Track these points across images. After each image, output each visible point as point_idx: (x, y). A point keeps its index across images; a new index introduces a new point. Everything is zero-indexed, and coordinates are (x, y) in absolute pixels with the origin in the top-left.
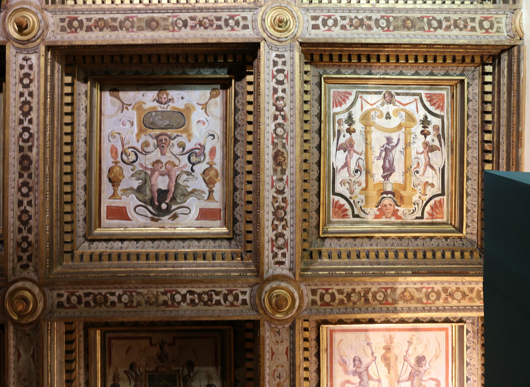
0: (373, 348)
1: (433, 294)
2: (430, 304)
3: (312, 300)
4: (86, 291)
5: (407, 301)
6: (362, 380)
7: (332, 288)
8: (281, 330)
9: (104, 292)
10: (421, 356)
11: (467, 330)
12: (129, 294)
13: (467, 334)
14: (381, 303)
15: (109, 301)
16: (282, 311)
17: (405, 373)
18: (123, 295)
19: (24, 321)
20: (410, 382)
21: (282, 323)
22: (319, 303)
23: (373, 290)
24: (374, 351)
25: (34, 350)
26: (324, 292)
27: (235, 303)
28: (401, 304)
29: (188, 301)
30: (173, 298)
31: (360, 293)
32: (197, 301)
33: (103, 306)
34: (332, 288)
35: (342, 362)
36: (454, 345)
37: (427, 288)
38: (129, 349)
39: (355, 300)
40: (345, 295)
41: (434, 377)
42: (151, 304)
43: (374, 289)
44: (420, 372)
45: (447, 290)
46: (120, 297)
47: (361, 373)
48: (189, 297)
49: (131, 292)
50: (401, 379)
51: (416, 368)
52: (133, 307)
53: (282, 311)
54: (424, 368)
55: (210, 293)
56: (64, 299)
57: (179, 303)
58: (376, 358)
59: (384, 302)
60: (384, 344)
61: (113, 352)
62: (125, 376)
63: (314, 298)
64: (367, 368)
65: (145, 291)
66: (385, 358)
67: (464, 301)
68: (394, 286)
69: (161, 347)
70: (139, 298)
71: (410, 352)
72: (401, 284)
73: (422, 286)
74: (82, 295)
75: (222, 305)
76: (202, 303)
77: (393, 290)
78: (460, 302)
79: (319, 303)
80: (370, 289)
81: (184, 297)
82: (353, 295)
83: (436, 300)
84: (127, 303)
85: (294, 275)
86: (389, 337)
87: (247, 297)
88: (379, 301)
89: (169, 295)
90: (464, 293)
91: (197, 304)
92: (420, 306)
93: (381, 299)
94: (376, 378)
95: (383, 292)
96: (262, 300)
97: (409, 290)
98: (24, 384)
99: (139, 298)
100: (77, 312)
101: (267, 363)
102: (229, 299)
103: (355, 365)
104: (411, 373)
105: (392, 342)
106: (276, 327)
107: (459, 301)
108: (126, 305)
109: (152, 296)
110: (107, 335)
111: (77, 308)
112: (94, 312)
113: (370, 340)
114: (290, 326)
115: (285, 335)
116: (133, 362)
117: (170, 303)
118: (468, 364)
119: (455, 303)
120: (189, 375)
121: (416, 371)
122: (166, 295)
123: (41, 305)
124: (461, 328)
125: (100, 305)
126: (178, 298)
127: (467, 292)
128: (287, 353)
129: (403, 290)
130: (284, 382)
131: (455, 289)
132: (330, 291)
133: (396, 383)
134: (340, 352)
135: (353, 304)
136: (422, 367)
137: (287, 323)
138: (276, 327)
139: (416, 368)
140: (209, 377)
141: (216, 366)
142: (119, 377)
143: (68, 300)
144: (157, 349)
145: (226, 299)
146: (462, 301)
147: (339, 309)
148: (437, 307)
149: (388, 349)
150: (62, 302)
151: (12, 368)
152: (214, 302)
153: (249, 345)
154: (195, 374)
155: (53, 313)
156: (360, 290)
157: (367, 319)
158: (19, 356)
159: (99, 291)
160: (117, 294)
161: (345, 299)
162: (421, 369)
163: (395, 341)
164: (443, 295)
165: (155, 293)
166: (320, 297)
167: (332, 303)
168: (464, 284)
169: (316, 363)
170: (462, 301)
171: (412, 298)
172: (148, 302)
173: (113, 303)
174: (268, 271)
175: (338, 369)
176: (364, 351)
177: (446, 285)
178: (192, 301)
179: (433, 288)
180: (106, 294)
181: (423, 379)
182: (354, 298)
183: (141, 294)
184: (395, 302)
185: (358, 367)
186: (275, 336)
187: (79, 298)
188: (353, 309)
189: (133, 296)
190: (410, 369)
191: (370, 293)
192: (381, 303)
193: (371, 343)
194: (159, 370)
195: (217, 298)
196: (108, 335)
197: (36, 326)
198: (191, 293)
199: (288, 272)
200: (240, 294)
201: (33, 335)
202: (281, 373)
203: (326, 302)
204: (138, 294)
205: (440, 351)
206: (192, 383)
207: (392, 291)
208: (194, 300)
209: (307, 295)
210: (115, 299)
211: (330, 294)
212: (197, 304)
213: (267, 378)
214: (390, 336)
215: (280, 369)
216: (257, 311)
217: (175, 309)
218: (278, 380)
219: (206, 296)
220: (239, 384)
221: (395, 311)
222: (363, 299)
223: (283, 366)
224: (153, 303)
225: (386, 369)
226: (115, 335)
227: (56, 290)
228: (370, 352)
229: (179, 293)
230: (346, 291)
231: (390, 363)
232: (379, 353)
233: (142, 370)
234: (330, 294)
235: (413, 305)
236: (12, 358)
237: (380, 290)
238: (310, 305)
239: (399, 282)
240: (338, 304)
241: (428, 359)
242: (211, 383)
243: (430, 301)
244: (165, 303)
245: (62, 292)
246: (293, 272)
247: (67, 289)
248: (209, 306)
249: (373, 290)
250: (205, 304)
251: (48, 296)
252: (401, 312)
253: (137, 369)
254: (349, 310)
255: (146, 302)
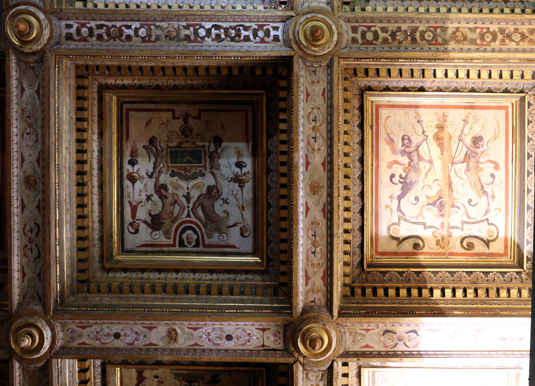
0: (424, 126)
1: (489, 34)
2: (485, 45)
3: (353, 38)
4: (99, 23)
5: (460, 41)
6: (411, 160)
7: (375, 26)
8: (317, 69)
9: (118, 24)
10: (478, 136)
11: (529, 102)
12: (147, 27)
13: (529, 107)
14: (429, 43)
15: (125, 35)
16: (318, 43)
17: (460, 154)
18: (139, 28)
19: (27, 49)
20: (465, 163)
21: (319, 59)
22: (360, 41)
23: (420, 29)
24: (425, 129)
25: (39, 84)
26: (366, 29)
27: (266, 39)
28: (452, 45)
29: (213, 36)
30: (196, 32)
31: (406, 31)
32: (223, 36)
33: (118, 40)
34: (375, 26)
35: (389, 140)
36: (514, 125)
37: (482, 29)
38: (149, 122)
39: (401, 40)
40: (389, 33)
41: (493, 159)
42: (171, 39)
43: (422, 27)
44: (477, 153)
45: (505, 31)
46: (136, 30)
47: (410, 153)
48: (214, 31)
49: (149, 26)
50: (455, 160)
51: (472, 149)
52: (151, 42)
53: (318, 43)
54: (481, 149)
55: (237, 28)
56: (73, 30)
57: (203, 38)
58: (427, 137)
59: (434, 42)
60: (437, 123)
61: (131, 124)
62: (144, 151)
63: (354, 35)
64: (418, 147)
65: (164, 24)
66: (437, 138)
67: (523, 43)
68: (445, 25)
69: (185, 121)
70: (159, 32)
71: (466, 131)
72: (452, 23)
73: (476, 25)
74: (94, 27)
75: (252, 41)
76: (229, 39)
77: (443, 29)
78: (519, 45)
79: (360, 41)
80: (418, 27)
81: (209, 31)
82: (398, 34)
83: (492, 41)
84: (145, 37)
85: (332, 8)
86: (442, 115)
87: (279, 33)
88: (427, 40)
89: (192, 29)
90: (524, 35)
91: (224, 39)
92: (473, 47)
93: (430, 39)
94: (428, 159)
95: (432, 32)
96: (296, 33)
97: (462, 30)
98: (29, 121)
99: (159, 32)
100: (88, 45)
101: (301, 105)
102: (259, 35)
103: (403, 145)
104: (466, 154)
105: (445, 121)
106: (312, 66)
107: (518, 43)
108: (143, 39)
109: (172, 30)
110: (124, 105)
111: (88, 41)
112: (108, 46)
113: (420, 117)
114: (327, 65)
115: (322, 74)
116: (153, 136)
117: (192, 37)
118: (529, 140)
119: (513, 45)
120: (216, 151)
121: (472, 152)
122: (189, 29)
123: (46, 32)
124: (523, 99)
125: (114, 39)
126: (202, 32)
127: (527, 34)
128: (323, 95)
129: (454, 30)
130: (320, 126)
131: (513, 30)
132: (373, 29)
133: (450, 165)
134: (386, 130)
135: (399, 44)
136: (479, 148)
137: (325, 60)
138: (312, 66)
139: (472, 149)
140: (239, 154)
141: (247, 141)
142: (138, 152)
143: (78, 31)
144: (181, 122)
145: (255, 35)
146: (521, 43)
147: (383, 48)
148: (493, 49)
149: (441, 128)
150: (71, 34)
151: (16, 246)
152: (242, 38)
153: (282, 105)
154: (222, 151)
155: (61, 45)
156: (406, 28)
157: (416, 87)
158: (23, 90)
159: (113, 23)
160: (133, 27)
161: (389, 38)
162: (478, 150)
163: (449, 119)
164: (500, 37)
165: (176, 27)
166: (362, 35)
167: (374, 42)
168: (523, 24)
169: (359, 134)
170: (521, 43)
171: (465, 38)
172: (168, 37)
173: (129, 37)
174: (303, 5)
175: (384, 148)
176: (414, 129)
177: (503, 25)
178: (218, 36)
179: (488, 28)
180: (121, 27)
181: (480, 161)
182: (400, 36)
183: (161, 28)
184: (445, 42)
185: (407, 147)
186: (310, 75)
187: (91, 30)
188: (399, 48)
189: (151, 30)
190: (465, 150)
191: (418, 32)
192: (429, 43)
193: (422, 121)
194: (183, 146)
195: (246, 33)
196: (126, 106)
197: (41, 56)
198: (217, 27)
199: (326, 6)
200: (271, 29)
201: (37, 64)
202: (317, 116)
203: (368, 40)
204: (157, 27)
205: (499, 131)
206: (219, 160)
207: (442, 31)
208: (220, 35)
209: (347, 32)
210: (131, 32)
211: (372, 32)
212: (224, 39)
213: (301, 121)
214: (444, 114)
215: (315, 111)
216: (291, 47)
217: (198, 44)
218: (313, 123)
219: (233, 31)
220: (271, 155)
221: (446, 51)
222: (409, 38)
223: (319, 109)
224: (174, 37)
225: (438, 150)
226: (134, 106)
227: (65, 20)
228: (421, 131)
229: (203, 27)
230: (390, 29)
231: (443, 144)
232: (431, 132)
233: (163, 145)
234: (372, 32)
235: (466, 47)
236: (14, 91)
237: (428, 29)
238: (350, 43)
239: (450, 19)
240: (382, 43)
241: (485, 140)
242: (241, 160)
243: (485, 43)
244: (187, 38)
245: (71, 22)
246: (331, 5)
247: (77, 19)
248: (237, 42)
249: (420, 29)
250: (233, 39)
251: (55, 24)
252: (452, 52)
253: (158, 144)
254: (394, 49)
255: (166, 36)
